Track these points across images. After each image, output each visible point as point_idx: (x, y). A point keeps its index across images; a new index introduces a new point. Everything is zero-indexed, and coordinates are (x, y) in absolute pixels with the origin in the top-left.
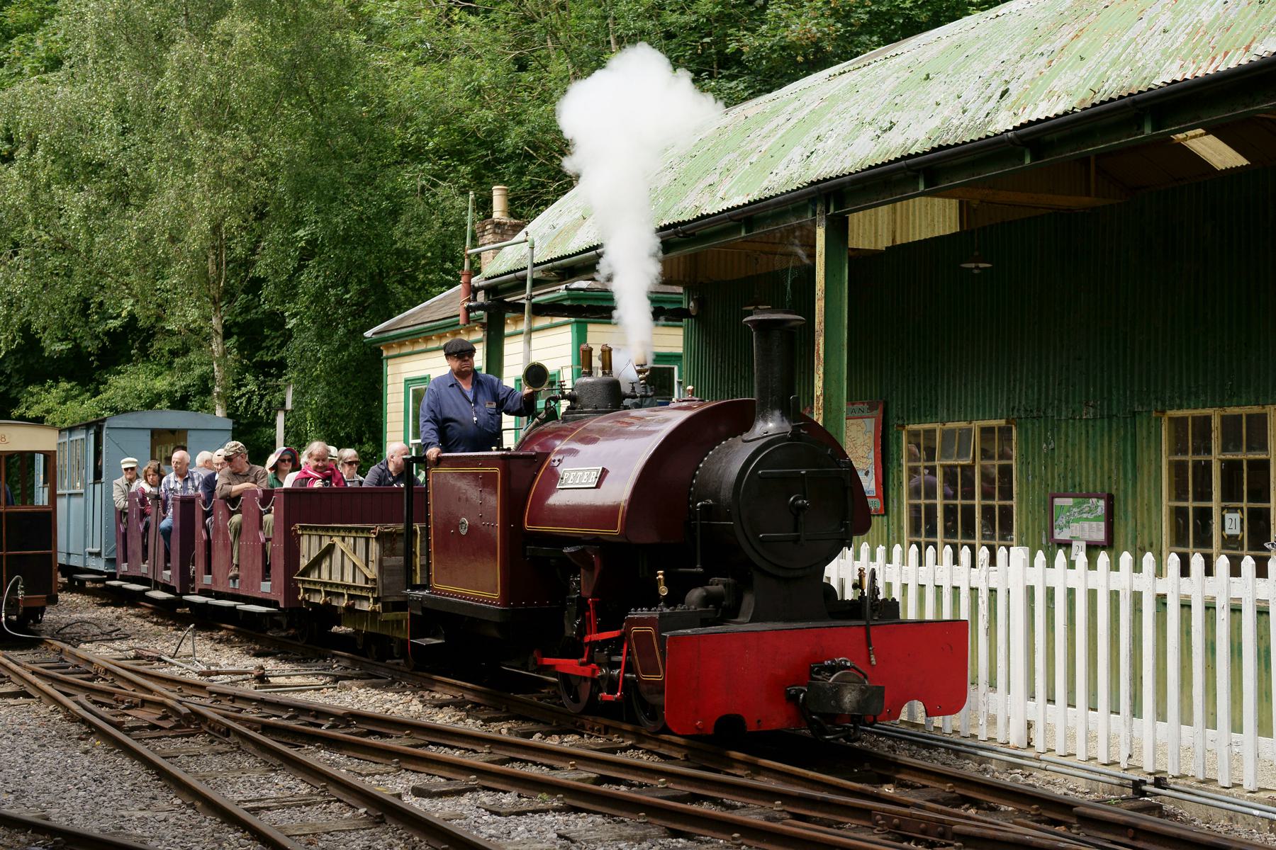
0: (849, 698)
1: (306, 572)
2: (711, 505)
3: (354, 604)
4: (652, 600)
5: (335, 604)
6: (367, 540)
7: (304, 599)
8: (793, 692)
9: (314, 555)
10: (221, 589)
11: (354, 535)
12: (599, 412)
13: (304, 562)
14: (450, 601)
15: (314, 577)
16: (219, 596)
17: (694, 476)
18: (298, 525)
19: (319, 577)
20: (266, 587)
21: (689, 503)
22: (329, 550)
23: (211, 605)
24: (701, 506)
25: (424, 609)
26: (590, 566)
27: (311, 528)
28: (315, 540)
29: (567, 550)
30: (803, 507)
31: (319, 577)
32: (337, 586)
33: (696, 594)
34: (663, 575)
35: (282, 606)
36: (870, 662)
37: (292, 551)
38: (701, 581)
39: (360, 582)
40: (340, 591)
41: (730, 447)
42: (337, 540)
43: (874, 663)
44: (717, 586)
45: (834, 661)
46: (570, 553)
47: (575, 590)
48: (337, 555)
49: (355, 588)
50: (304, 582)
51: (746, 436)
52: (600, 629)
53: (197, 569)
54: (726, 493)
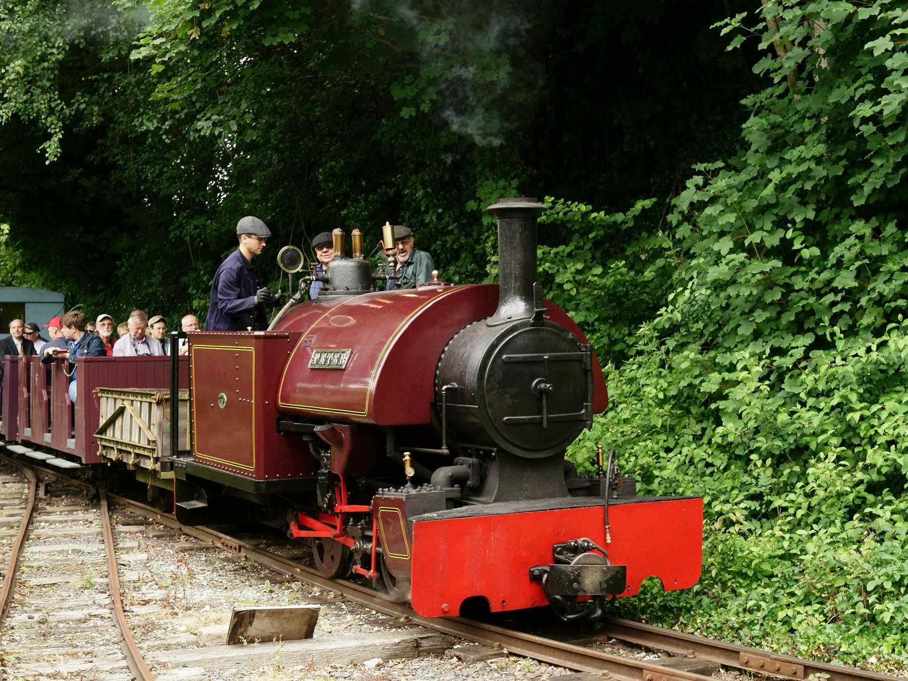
0: (591, 581)
1: (103, 430)
2: (456, 389)
3: (139, 462)
4: (399, 480)
5: (125, 461)
6: (150, 403)
7: (102, 455)
8: (537, 573)
9: (109, 416)
10: (37, 441)
11: (140, 399)
12: (351, 294)
13: (102, 421)
14: (210, 470)
15: (109, 435)
16: (38, 448)
17: (440, 360)
18: (98, 389)
19: (114, 436)
20: (71, 445)
21: (435, 385)
22: (121, 411)
23: (28, 457)
24: (447, 389)
25: (188, 476)
26: (340, 443)
27: (108, 391)
28: (111, 401)
29: (318, 429)
30: (545, 391)
31: (114, 436)
32: (127, 445)
33: (442, 474)
34: (410, 456)
35: (84, 462)
36: (605, 540)
37: (93, 411)
38: (447, 461)
39: (144, 443)
40: (128, 449)
41: (474, 331)
42: (126, 404)
43: (609, 541)
44: (463, 466)
45: (576, 542)
46: (322, 432)
47: (326, 466)
48: (127, 414)
49: (140, 447)
50: (101, 439)
51: (490, 321)
52: (350, 502)
53: (20, 419)
54: (471, 377)
